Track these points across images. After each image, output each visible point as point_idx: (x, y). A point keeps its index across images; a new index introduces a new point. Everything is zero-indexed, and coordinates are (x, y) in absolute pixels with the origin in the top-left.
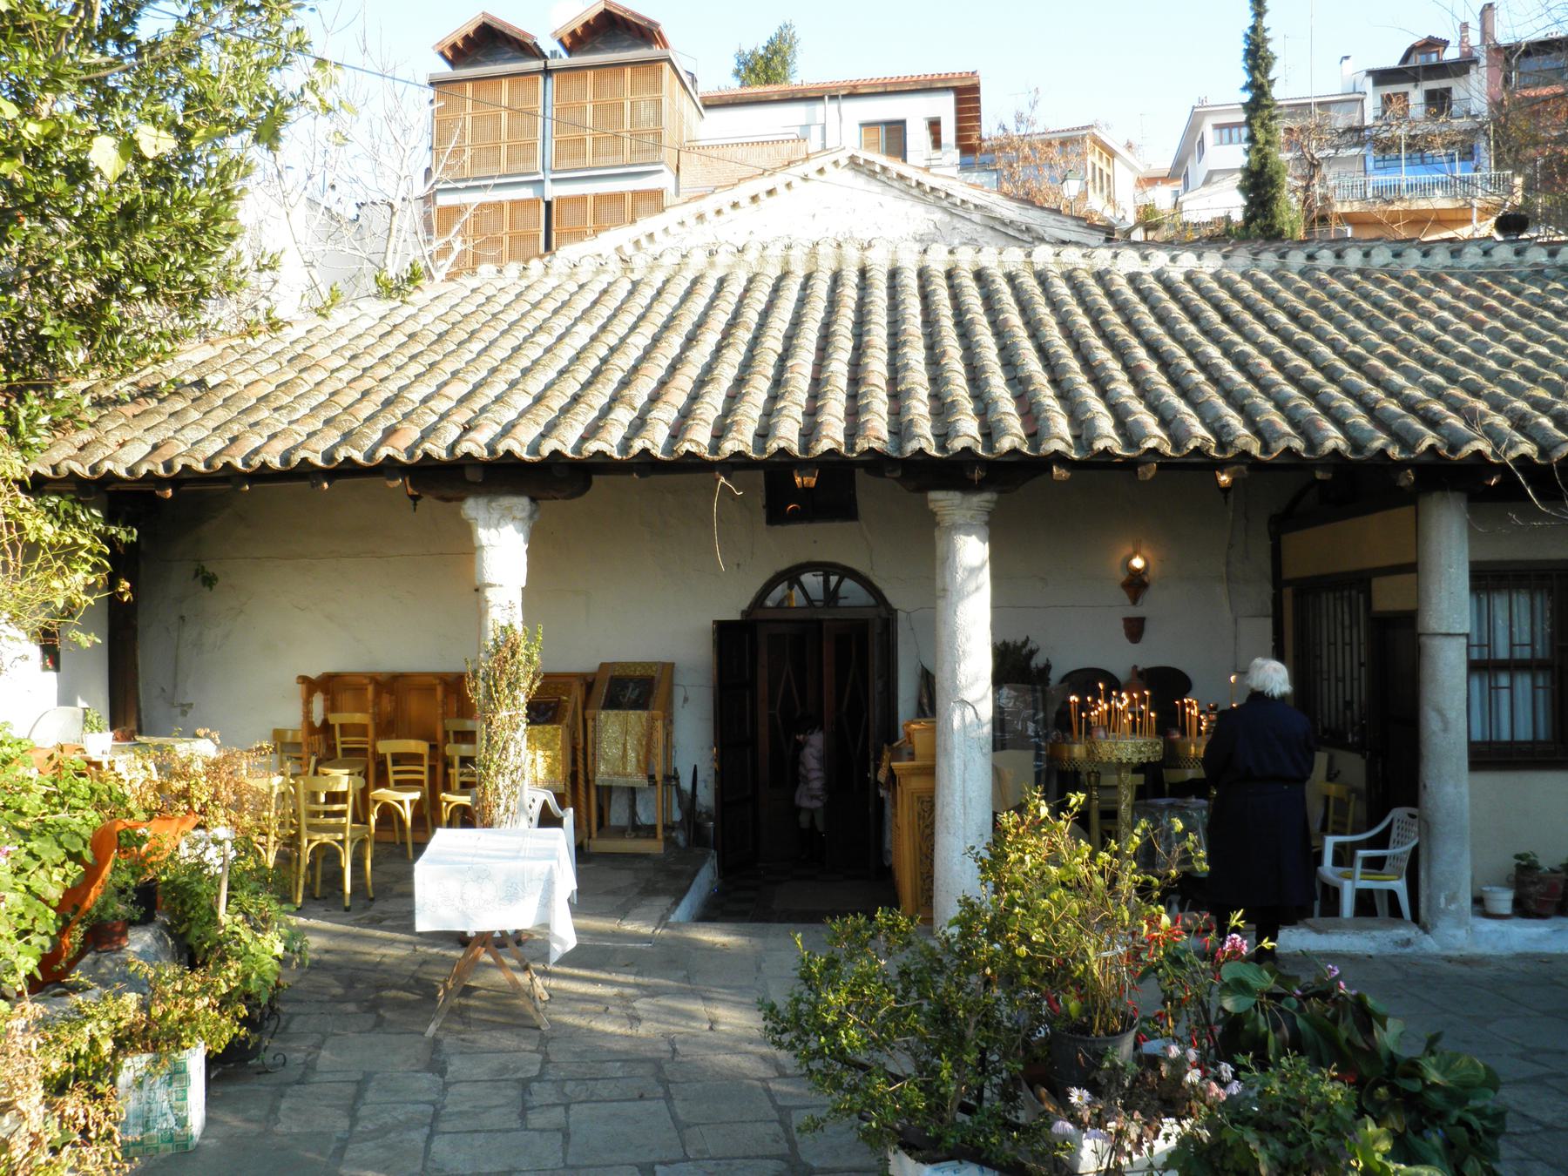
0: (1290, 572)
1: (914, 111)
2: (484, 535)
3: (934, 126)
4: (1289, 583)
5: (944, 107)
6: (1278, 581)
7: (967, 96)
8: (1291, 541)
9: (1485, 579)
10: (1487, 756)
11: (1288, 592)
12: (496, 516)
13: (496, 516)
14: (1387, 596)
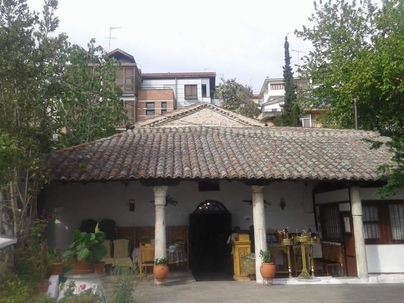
0: (317, 202)
1: (199, 82)
2: (156, 195)
3: (204, 87)
4: (319, 205)
5: (207, 82)
6: (315, 205)
7: (212, 78)
8: (317, 196)
9: (365, 204)
10: (368, 242)
11: (318, 208)
12: (160, 190)
13: (160, 190)
14: (344, 208)
